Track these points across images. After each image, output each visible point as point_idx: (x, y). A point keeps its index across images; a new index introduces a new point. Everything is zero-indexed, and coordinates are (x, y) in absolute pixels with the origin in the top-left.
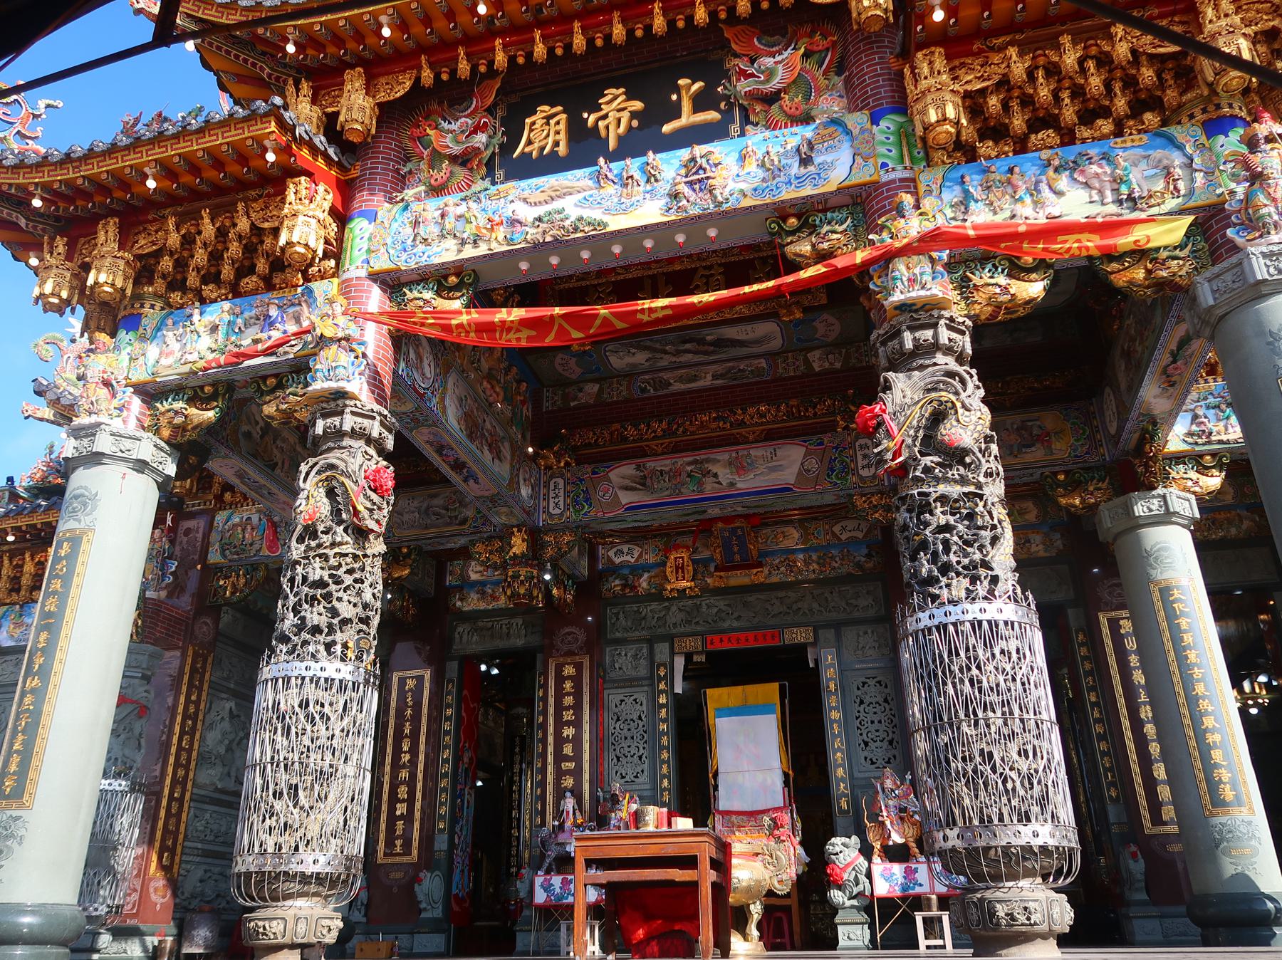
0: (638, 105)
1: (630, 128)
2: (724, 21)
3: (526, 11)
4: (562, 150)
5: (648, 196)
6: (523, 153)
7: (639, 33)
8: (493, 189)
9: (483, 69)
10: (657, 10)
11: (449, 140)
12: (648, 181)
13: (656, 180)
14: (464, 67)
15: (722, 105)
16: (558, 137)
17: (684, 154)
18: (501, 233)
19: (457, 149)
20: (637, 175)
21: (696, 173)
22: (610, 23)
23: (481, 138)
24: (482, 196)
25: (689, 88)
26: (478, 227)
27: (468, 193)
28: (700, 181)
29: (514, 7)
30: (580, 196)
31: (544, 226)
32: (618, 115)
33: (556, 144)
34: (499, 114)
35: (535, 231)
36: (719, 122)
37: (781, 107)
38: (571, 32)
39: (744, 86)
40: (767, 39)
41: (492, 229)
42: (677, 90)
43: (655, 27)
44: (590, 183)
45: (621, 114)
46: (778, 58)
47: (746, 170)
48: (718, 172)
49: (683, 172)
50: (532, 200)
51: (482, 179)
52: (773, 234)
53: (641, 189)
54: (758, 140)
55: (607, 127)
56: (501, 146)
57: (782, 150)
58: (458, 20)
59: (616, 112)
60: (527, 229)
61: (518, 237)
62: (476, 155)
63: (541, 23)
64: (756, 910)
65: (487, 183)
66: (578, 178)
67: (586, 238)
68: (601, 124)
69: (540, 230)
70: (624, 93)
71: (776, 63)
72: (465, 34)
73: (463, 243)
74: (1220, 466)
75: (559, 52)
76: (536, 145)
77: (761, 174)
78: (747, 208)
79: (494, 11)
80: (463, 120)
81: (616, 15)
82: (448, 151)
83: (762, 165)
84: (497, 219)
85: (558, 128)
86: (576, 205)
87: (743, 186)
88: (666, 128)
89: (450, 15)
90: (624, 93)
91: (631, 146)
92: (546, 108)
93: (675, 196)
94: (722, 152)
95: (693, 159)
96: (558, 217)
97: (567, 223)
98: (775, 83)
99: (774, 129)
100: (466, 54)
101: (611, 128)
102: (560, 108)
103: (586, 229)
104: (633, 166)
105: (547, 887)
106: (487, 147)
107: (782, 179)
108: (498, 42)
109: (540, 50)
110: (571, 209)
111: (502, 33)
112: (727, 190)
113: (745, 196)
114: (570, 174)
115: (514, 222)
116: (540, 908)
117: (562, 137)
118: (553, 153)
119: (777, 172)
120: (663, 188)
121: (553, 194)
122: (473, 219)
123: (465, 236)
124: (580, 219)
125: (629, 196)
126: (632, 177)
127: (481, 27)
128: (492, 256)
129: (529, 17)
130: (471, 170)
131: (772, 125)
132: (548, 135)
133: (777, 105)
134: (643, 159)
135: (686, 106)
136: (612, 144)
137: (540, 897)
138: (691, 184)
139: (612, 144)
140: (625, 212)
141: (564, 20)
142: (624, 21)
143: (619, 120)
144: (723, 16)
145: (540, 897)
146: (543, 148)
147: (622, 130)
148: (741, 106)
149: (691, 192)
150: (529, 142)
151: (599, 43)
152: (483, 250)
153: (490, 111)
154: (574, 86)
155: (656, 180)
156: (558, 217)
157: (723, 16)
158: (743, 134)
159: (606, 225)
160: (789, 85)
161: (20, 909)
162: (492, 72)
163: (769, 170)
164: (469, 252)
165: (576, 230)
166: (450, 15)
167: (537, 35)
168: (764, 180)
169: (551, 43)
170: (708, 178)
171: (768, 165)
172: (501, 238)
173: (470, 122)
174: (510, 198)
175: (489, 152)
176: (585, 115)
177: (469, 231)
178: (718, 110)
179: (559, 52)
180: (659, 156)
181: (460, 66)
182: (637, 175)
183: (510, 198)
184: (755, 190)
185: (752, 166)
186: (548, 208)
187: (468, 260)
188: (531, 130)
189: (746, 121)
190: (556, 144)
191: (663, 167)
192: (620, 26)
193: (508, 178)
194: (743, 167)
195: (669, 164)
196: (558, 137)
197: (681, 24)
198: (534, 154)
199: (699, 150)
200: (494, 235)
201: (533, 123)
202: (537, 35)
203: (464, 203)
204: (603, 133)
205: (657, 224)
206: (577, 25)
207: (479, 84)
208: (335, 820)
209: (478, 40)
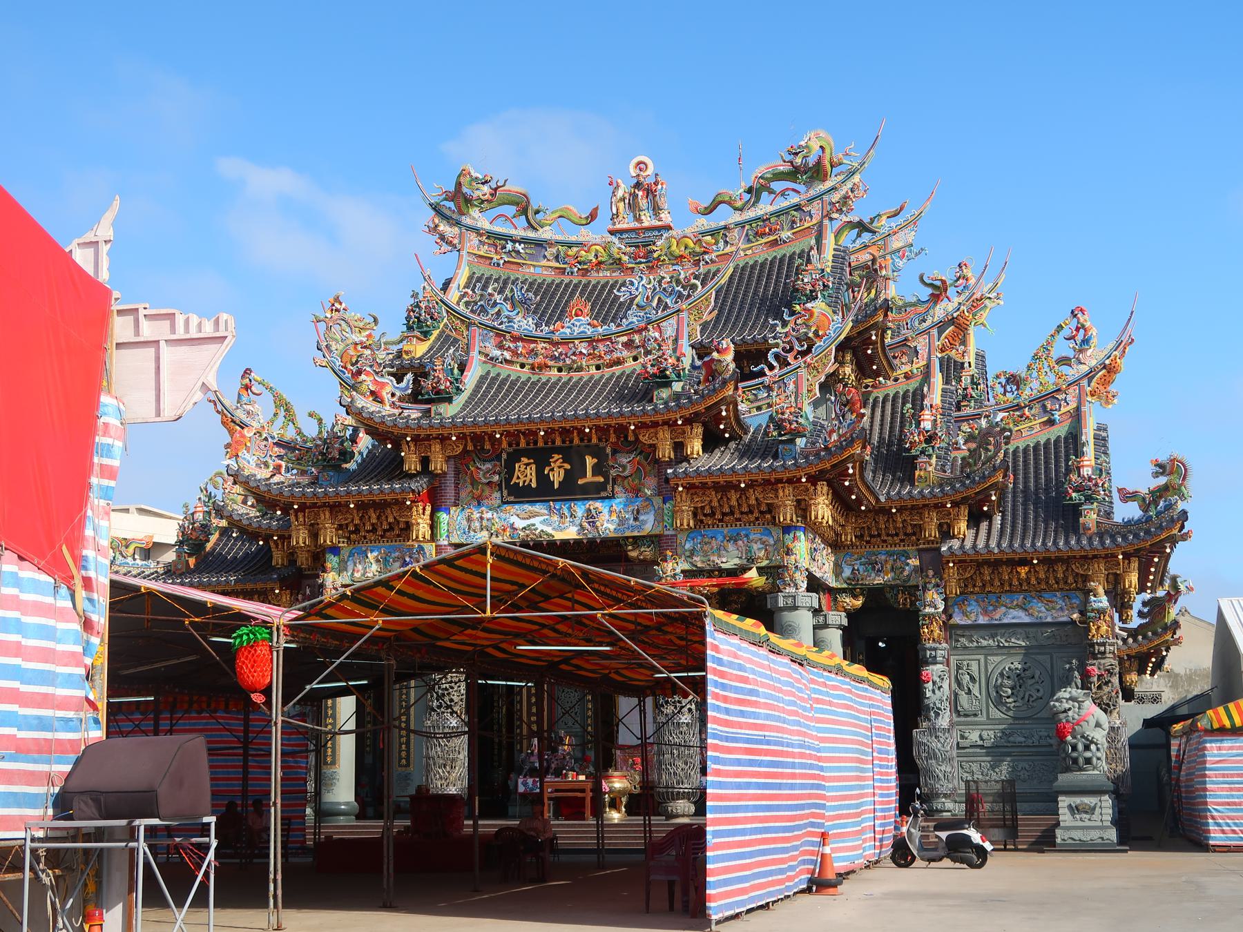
64: (624, 800)
74: (862, 594)
105: (525, 784)
116: (521, 794)
137: (521, 789)
145: (521, 789)
161: (340, 804)
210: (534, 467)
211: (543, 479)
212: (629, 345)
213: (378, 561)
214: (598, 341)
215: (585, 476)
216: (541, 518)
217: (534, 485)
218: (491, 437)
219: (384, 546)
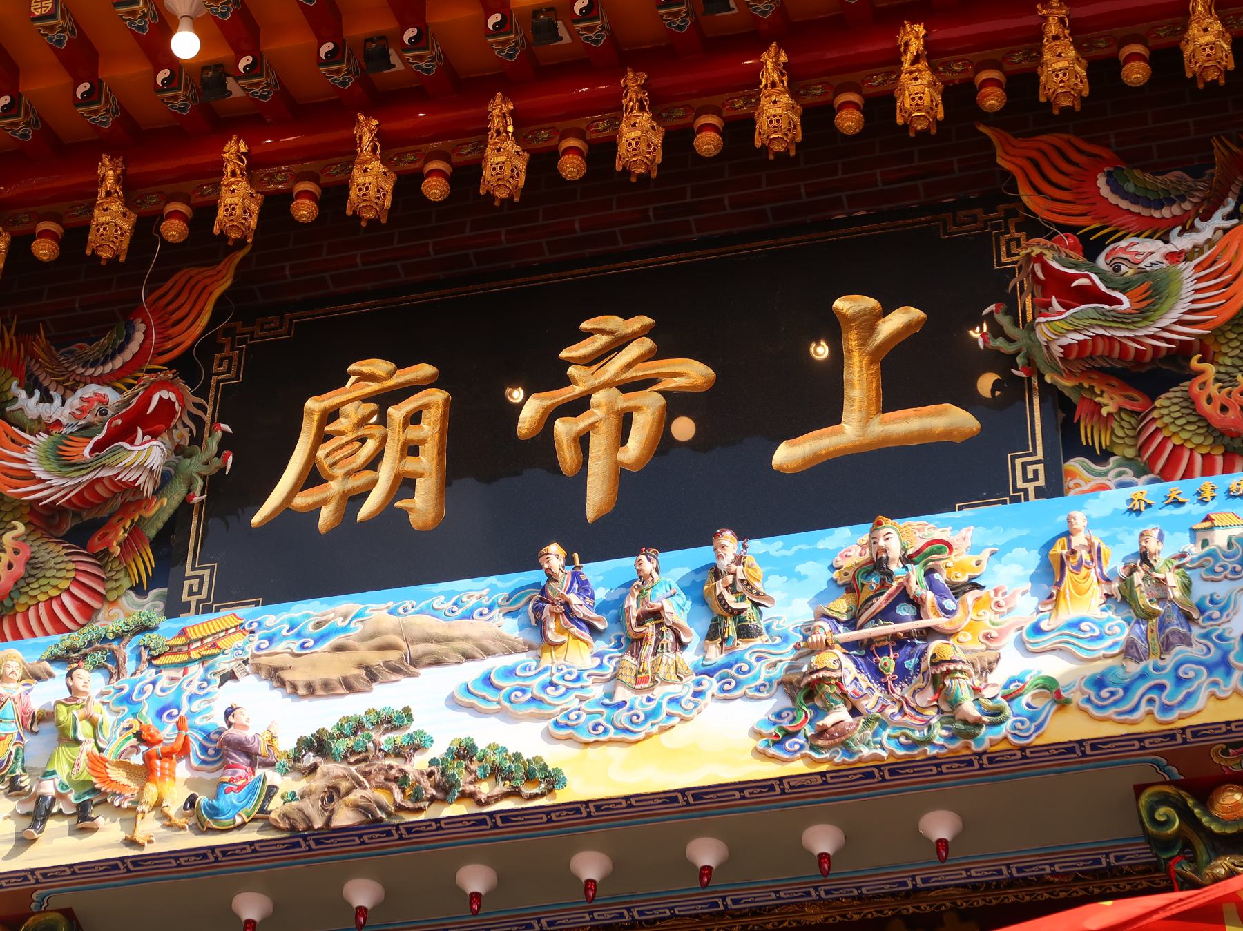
0: (692, 373)
1: (663, 442)
2: (993, 119)
3: (333, 57)
4: (422, 506)
5: (711, 685)
6: (285, 511)
7: (707, 143)
8: (168, 629)
9: (173, 231)
10: (770, 73)
11: (34, 455)
12: (714, 632)
13: (745, 632)
14: (111, 223)
15: (985, 383)
16: (411, 464)
17: (846, 544)
18: (177, 785)
19: (56, 485)
20: (677, 609)
21: (887, 614)
22: (613, 107)
23: (148, 454)
24: (126, 651)
25: (869, 322)
26: (97, 763)
27: (77, 638)
28: (900, 642)
29: (294, 45)
30: (471, 672)
31: (334, 769)
32: (623, 401)
33: (405, 485)
34: (221, 376)
35: (299, 785)
36: (970, 443)
37: (1191, 403)
38: (480, 132)
39: (1059, 328)
40: (1138, 179)
41: (146, 773)
42: (832, 328)
43: (763, 125)
44: (510, 628)
45: (635, 399)
46: (1181, 243)
47: (1068, 612)
48: (968, 615)
49: (841, 606)
50: (298, 676)
51: (139, 590)
52: (1166, 844)
53: (689, 657)
54: (1105, 511)
55: (583, 441)
56: (214, 483)
57: (1195, 550)
58: (105, 74)
59: (615, 394)
60: (273, 777)
61: (235, 803)
62: (125, 509)
63: (377, 98)
65: (149, 607)
66: (472, 606)
67: (477, 821)
68: (564, 429)
69: (317, 783)
70: (649, 332)
71: (1173, 257)
72: (125, 119)
73: (40, 812)
75: (435, 189)
76: (335, 487)
77: (1119, 629)
78: (1069, 748)
79: (223, 53)
80: (91, 390)
81: (633, 83)
82: (29, 491)
83: (1123, 598)
84: (167, 732)
85: (413, 433)
86: (454, 703)
87: (1055, 667)
88: (786, 455)
89: (80, 56)
90: (649, 332)
91: (660, 509)
92: (380, 366)
93: (808, 690)
94: (984, 545)
95: (878, 565)
96: (385, 740)
97: (419, 763)
98: (1172, 321)
99: (1166, 475)
100: (125, 181)
101: (598, 445)
102: (425, 370)
103: (484, 789)
104: (668, 576)
106: (165, 480)
107: (1196, 651)
108: (234, 149)
109: (371, 182)
110: (436, 711)
111: (247, 121)
112: (999, 677)
113: (1061, 702)
114: (440, 594)
115: (226, 750)
117: (427, 463)
118: (391, 515)
119: (1176, 625)
120: (767, 658)
121: (376, 659)
122: (84, 731)
123: (49, 788)
124: (464, 753)
125: (645, 681)
126: (656, 615)
127: (180, 100)
128: (136, 868)
129: (342, 76)
130: (102, 557)
131: (1157, 463)
132: (373, 463)
133: (1175, 394)
134: (701, 555)
135: (859, 383)
136: (597, 496)
138: (866, 651)
139: (597, 496)
140: (626, 736)
141: (459, 90)
142: (658, 103)
143: (625, 421)
144: (993, 100)
146: (358, 497)
147: (634, 449)
148: (1051, 394)
149: (865, 681)
150: (313, 477)
151: (571, 167)
152: (106, 841)
153: (189, 367)
154: (481, 307)
155: (745, 632)
156: (385, 740)
157: (993, 100)
158: (1054, 487)
159: (553, 780)
160: (1218, 332)
162: (205, 242)
163: (1147, 615)
164: (58, 847)
165: (446, 790)
166: (80, 56)
167: (366, 131)
168: (1130, 651)
169: (409, 162)
170: (929, 633)
171: (1144, 600)
172: (174, 805)
173: (113, 397)
174: (224, 663)
175: (168, 504)
176: (517, 395)
177: (63, 772)
178: (968, 400)
179: (435, 189)
180: (756, 545)
181: (100, 217)
182: (677, 609)
183: (224, 663)
184: (1099, 682)
185: (1086, 601)
186: (354, 706)
187: (48, 874)
188: (323, 437)
189: (1068, 441)
190: (405, 485)
191: (771, 586)
192: (645, 118)
193: (229, 592)
194: (1052, 599)
195: (794, 579)
196: (411, 464)
197: (849, 121)
198: (326, 516)
199: (899, 536)
200: (151, 792)
201: (332, 415)
202: (366, 131)
203: (60, 672)
204: (567, 457)
205: (741, 787)
206: (499, 109)
207: (159, 279)
208: (969, 646)
209: (172, 135)
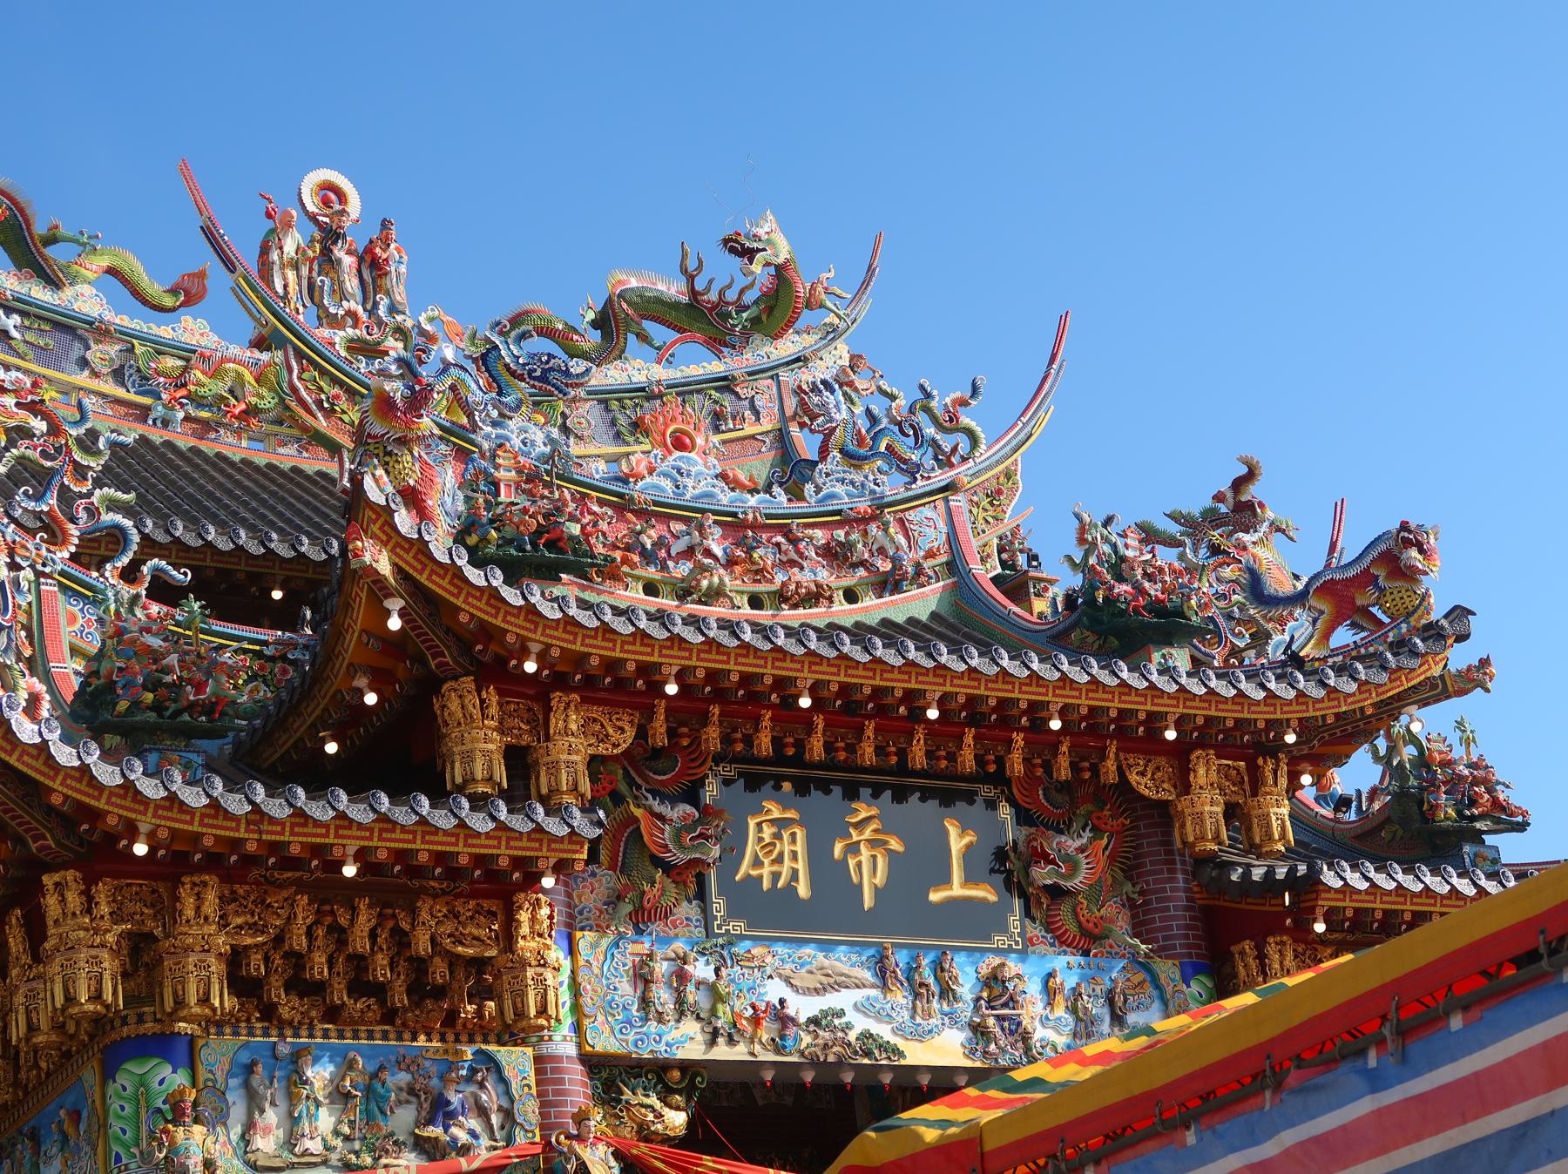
74: (688, 1092)
210: (800, 834)
211: (830, 872)
212: (835, 555)
213: (340, 1097)
214: (755, 526)
215: (946, 880)
216: (857, 995)
217: (803, 890)
218: (1039, 725)
219: (366, 1048)
